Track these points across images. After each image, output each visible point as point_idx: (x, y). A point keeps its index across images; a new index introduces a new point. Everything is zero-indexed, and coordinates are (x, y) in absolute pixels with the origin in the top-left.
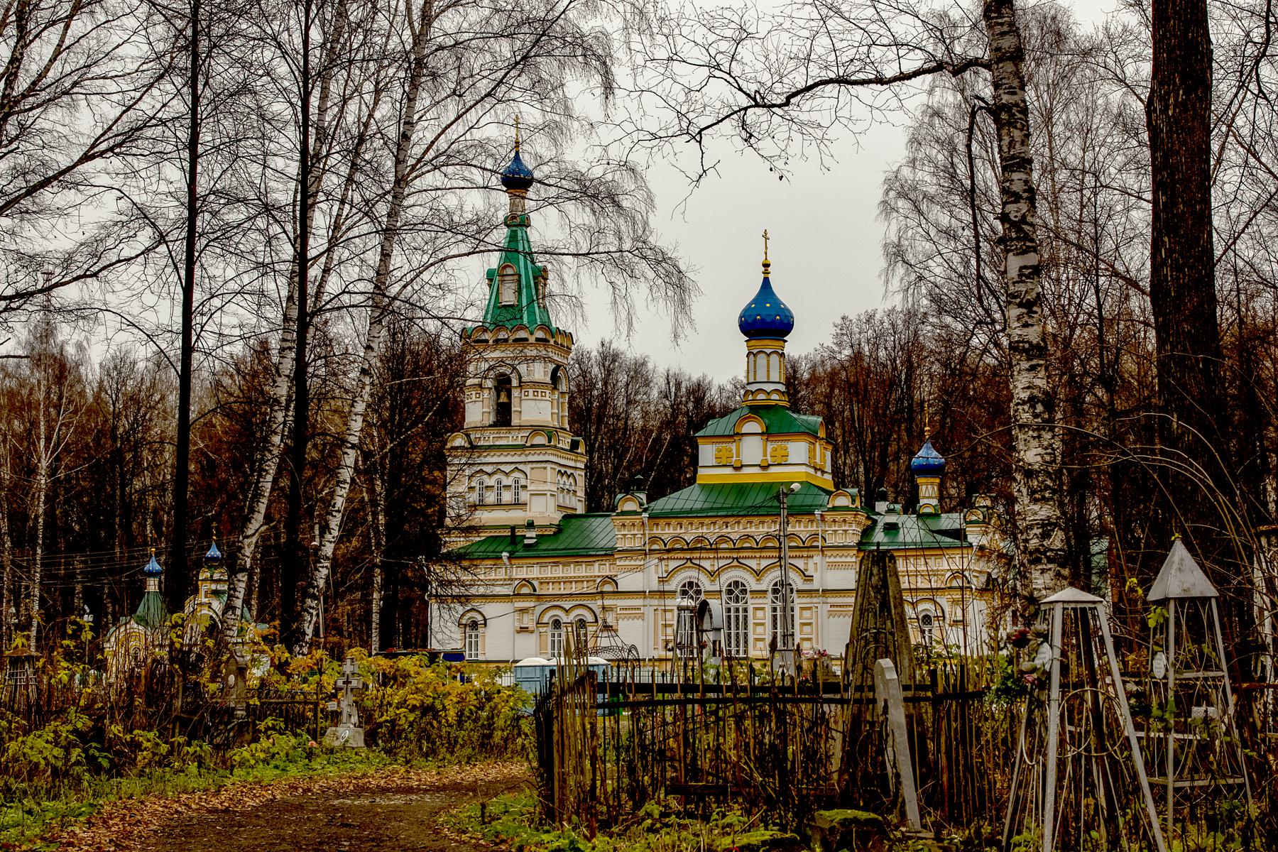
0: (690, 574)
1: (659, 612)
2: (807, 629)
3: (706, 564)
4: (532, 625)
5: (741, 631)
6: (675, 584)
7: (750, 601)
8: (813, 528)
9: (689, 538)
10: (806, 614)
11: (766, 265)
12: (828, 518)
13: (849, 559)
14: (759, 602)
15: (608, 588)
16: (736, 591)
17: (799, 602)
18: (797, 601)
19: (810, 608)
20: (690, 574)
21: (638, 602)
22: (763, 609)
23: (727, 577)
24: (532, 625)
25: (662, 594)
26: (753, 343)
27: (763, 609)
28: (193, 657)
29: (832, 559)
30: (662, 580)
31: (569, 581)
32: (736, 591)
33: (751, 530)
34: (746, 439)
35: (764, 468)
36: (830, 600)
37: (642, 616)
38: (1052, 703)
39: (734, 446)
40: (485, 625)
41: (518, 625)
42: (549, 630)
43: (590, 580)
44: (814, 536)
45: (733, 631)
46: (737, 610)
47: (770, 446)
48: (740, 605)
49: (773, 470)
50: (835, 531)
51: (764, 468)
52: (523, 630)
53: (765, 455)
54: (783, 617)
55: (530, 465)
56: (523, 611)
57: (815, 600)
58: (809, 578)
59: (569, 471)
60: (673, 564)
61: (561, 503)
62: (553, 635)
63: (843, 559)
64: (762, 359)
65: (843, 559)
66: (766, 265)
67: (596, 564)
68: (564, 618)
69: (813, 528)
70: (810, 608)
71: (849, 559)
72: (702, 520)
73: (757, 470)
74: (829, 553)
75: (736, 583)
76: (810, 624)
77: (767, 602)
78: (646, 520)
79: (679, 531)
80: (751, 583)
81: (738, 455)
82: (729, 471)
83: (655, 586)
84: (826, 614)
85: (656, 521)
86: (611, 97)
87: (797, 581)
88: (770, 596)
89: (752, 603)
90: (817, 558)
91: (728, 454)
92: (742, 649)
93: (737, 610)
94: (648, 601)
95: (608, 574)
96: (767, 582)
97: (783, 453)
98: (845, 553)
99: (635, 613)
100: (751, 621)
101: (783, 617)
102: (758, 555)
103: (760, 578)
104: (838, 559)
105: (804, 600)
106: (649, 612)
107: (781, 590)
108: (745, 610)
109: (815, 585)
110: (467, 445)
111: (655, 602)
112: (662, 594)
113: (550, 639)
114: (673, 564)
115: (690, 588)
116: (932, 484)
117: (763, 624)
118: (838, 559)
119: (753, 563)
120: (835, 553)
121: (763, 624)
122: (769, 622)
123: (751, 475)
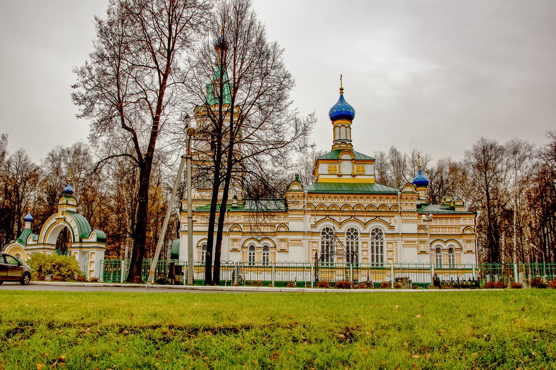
0: (328, 224)
1: (311, 243)
2: (390, 254)
3: (337, 219)
4: (239, 248)
5: (380, 254)
6: (319, 229)
7: (359, 239)
8: (395, 202)
11: (342, 89)
12: (404, 197)
13: (414, 218)
15: (282, 229)
16: (352, 233)
17: (385, 239)
18: (385, 239)
19: (391, 243)
20: (328, 224)
22: (366, 243)
24: (239, 248)
25: (313, 234)
26: (335, 123)
27: (366, 243)
29: (405, 218)
30: (312, 226)
32: (352, 233)
33: (361, 201)
34: (343, 162)
36: (404, 239)
37: (302, 245)
38: (154, 271)
41: (231, 248)
42: (247, 251)
44: (396, 206)
45: (375, 254)
46: (352, 243)
48: (379, 241)
49: (357, 177)
50: (406, 204)
51: (354, 176)
52: (235, 250)
54: (377, 250)
56: (235, 240)
57: (396, 239)
58: (392, 228)
60: (318, 218)
63: (411, 218)
64: (337, 129)
66: (342, 89)
68: (257, 244)
70: (391, 243)
71: (414, 218)
73: (350, 177)
74: (404, 215)
75: (352, 229)
76: (392, 251)
77: (369, 239)
78: (306, 194)
79: (322, 201)
80: (361, 229)
81: (340, 169)
82: (336, 177)
83: (309, 229)
84: (402, 246)
85: (311, 195)
87: (385, 229)
88: (346, 236)
89: (361, 239)
90: (397, 217)
91: (335, 169)
92: (380, 263)
93: (377, 243)
94: (306, 237)
96: (369, 229)
97: (363, 170)
98: (412, 215)
99: (299, 243)
100: (385, 250)
101: (377, 250)
102: (365, 215)
104: (408, 218)
105: (389, 239)
106: (305, 242)
107: (377, 233)
109: (396, 231)
110: (7, 257)
111: (309, 237)
112: (313, 234)
113: (248, 255)
114: (318, 218)
115: (327, 232)
117: (366, 251)
118: (408, 218)
119: (362, 219)
120: (407, 215)
121: (366, 251)
123: (347, 179)
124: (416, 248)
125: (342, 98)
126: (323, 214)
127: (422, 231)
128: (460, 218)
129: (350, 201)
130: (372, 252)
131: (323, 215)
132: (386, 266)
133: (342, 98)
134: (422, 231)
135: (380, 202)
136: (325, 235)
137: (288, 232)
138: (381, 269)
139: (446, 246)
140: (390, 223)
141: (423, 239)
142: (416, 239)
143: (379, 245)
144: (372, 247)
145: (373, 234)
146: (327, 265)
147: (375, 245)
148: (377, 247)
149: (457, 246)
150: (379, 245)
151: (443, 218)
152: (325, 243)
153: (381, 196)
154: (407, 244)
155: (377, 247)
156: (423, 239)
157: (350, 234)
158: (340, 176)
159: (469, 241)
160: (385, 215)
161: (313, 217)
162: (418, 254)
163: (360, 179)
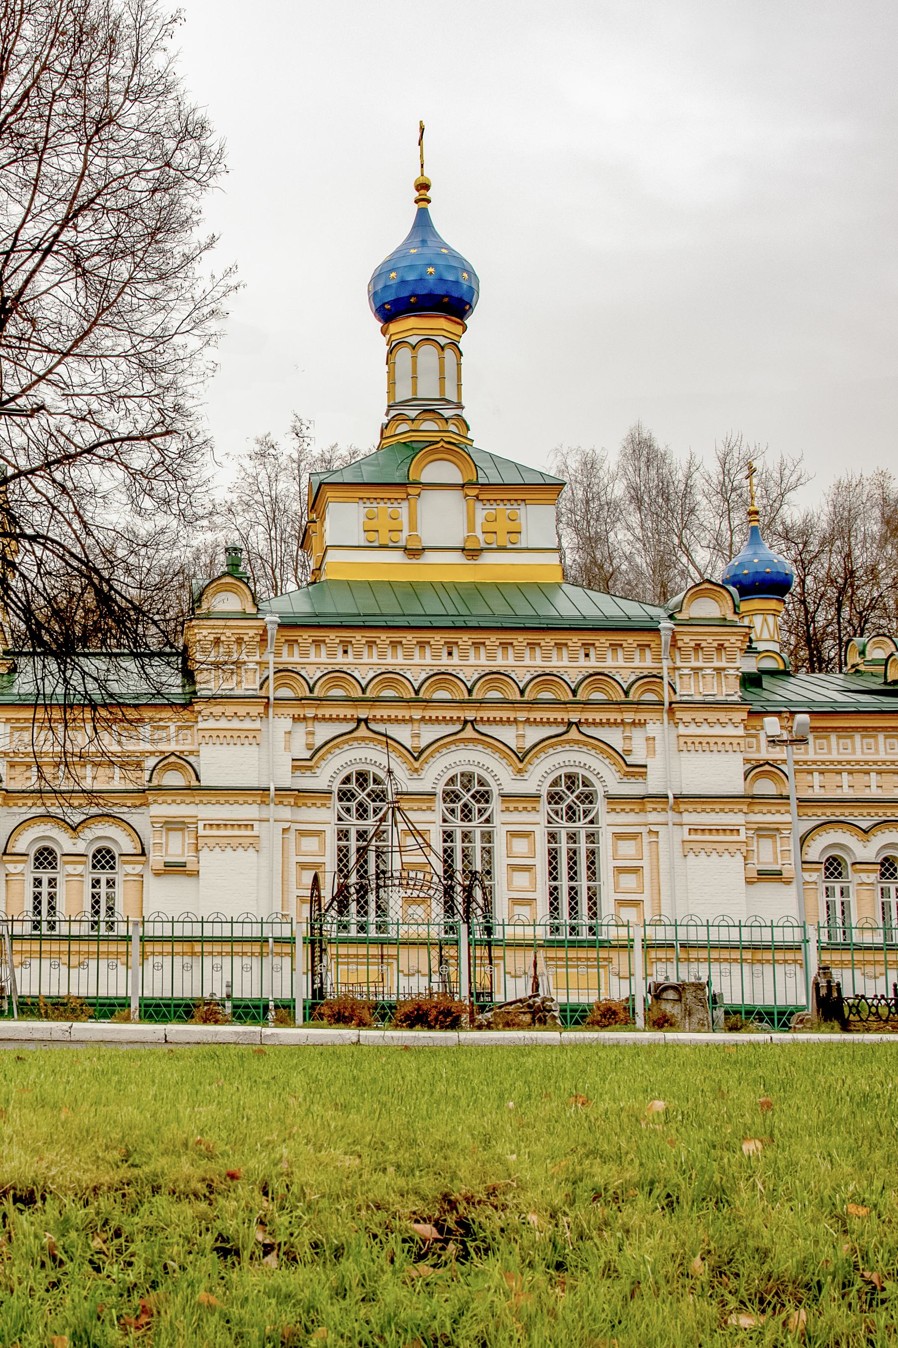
0: (367, 756)
1: (292, 835)
3: (402, 733)
5: (583, 883)
6: (328, 775)
7: (498, 819)
8: (646, 662)
9: (364, 675)
10: (627, 848)
11: (423, 186)
13: (730, 731)
14: (520, 819)
15: (173, 779)
16: (468, 797)
17: (608, 821)
19: (634, 836)
21: (248, 811)
26: (394, 327)
29: (693, 730)
31: (861, 769)
32: (468, 797)
36: (687, 818)
37: (254, 844)
39: (403, 510)
44: (652, 679)
45: (564, 884)
47: (481, 513)
49: (489, 558)
51: (472, 553)
53: (471, 526)
57: (653, 817)
58: (638, 771)
60: (324, 732)
62: (38, 882)
63: (718, 730)
64: (404, 354)
65: (718, 730)
66: (423, 186)
68: (64, 842)
69: (646, 662)
70: (634, 836)
71: (730, 731)
72: (396, 636)
73: (456, 558)
74: (687, 716)
76: (636, 870)
77: (537, 821)
78: (272, 630)
80: (502, 777)
81: (413, 526)
82: (397, 557)
85: (292, 634)
87: (608, 779)
89: (503, 820)
91: (394, 525)
93: (572, 837)
94: (274, 811)
95: (173, 747)
96: (538, 777)
97: (512, 527)
98: (723, 716)
99: (242, 837)
101: (572, 871)
102: (522, 716)
103: (516, 770)
104: (705, 730)
106: (269, 834)
107: (571, 797)
108: (488, 837)
109: (653, 785)
111: (286, 813)
113: (88, 890)
114: (324, 732)
115: (361, 792)
116: (775, 613)
117: (528, 868)
118: (705, 730)
119: (508, 735)
120: (700, 716)
121: (528, 868)
124: (739, 858)
125: (423, 221)
126: (342, 712)
127: (766, 787)
130: (553, 874)
131: (555, 722)
132: (609, 933)
133: (423, 221)
134: (766, 787)
136: (353, 805)
137: (196, 790)
138: (592, 945)
140: (629, 752)
141: (769, 818)
143: (583, 846)
144: (553, 855)
146: (362, 928)
147: (564, 846)
148: (573, 855)
150: (583, 846)
152: (353, 835)
154: (702, 841)
155: (573, 855)
156: (769, 818)
158: (414, 552)
161: (301, 728)
163: (498, 565)
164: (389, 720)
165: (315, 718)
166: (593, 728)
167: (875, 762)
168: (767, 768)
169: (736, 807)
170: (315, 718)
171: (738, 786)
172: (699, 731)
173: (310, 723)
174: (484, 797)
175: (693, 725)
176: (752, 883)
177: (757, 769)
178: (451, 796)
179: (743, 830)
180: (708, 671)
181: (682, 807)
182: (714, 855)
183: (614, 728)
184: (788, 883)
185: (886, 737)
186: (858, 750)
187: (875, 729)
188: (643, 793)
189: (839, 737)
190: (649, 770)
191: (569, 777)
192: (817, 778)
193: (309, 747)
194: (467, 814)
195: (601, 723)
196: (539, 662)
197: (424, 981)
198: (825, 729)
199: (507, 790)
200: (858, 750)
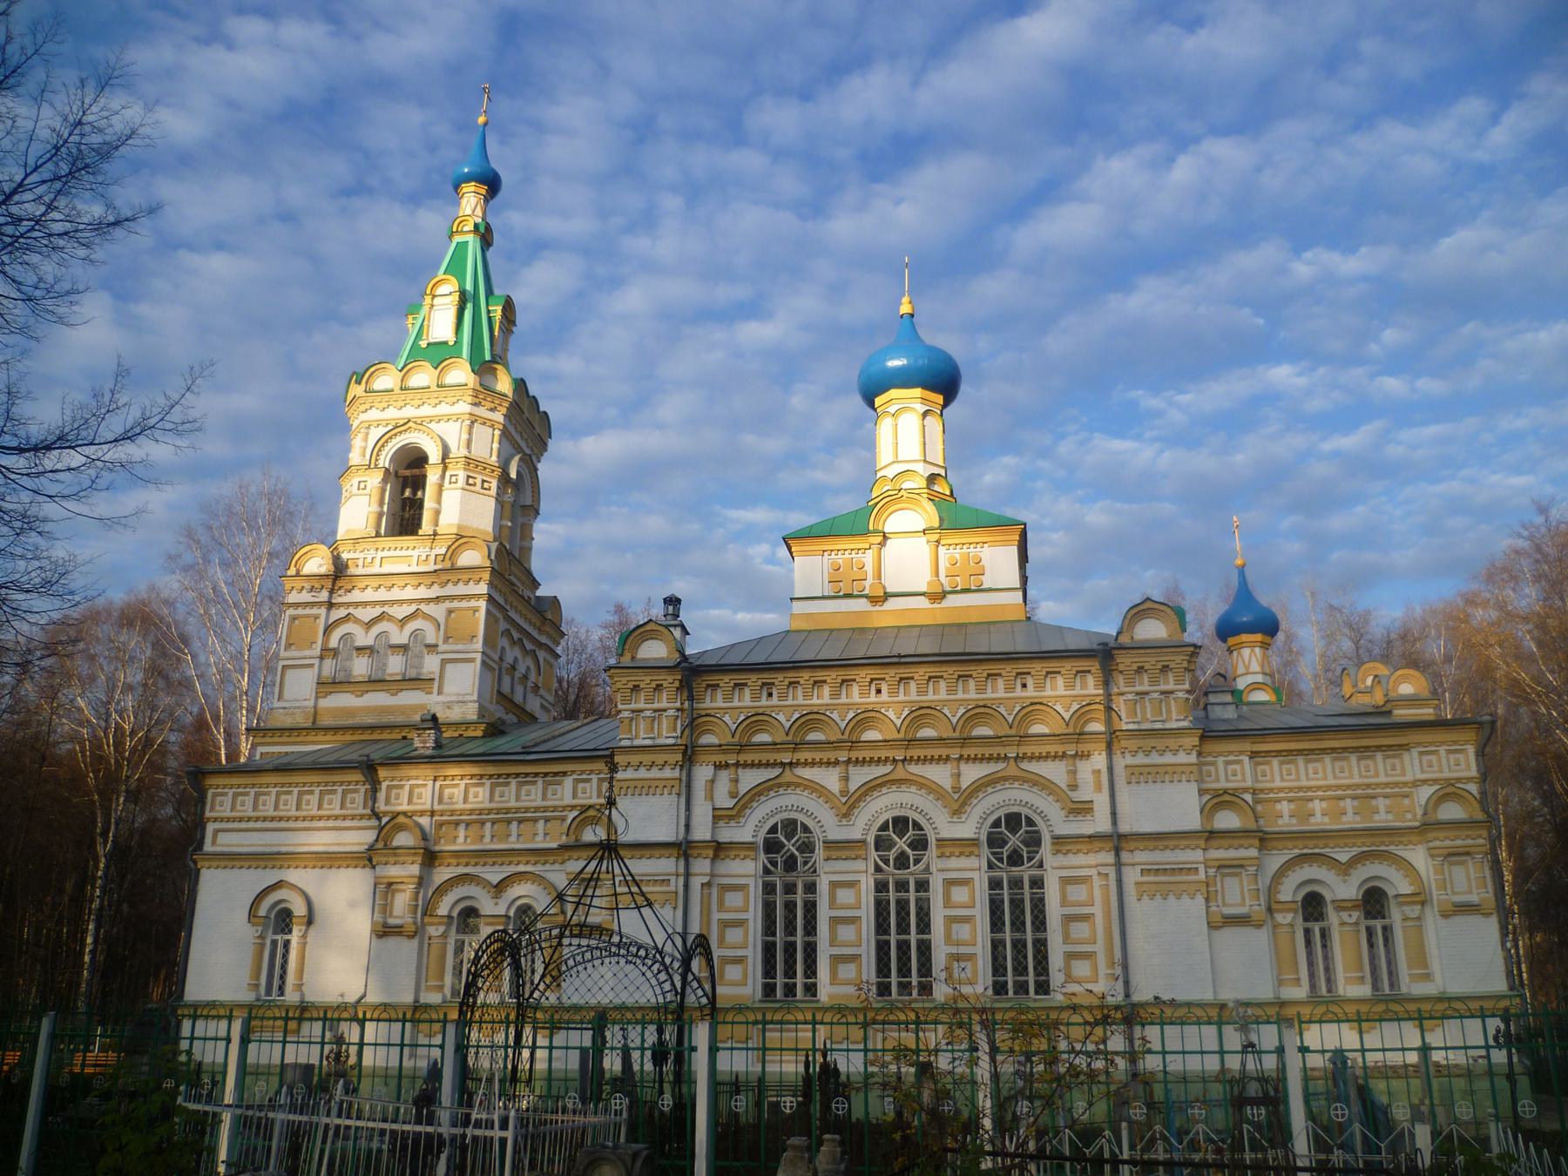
13: (1182, 758)
22: (852, 884)
23: (883, 806)
27: (852, 884)
28: (1272, 1093)
35: (943, 595)
36: (1215, 854)
40: (310, 921)
43: (549, 815)
48: (1026, 872)
49: (952, 601)
55: (448, 605)
59: (529, 646)
61: (506, 689)
67: (568, 782)
71: (1182, 758)
73: (923, 602)
77: (975, 869)
82: (861, 605)
86: (47, 527)
96: (864, 824)
100: (823, 913)
122: (981, 914)
124: (1200, 899)
127: (1227, 820)
128: (1405, 747)
129: (775, 701)
134: (1227, 820)
135: (1019, 692)
139: (1342, 888)
141: (1232, 853)
142: (1198, 855)
143: (799, 898)
145: (881, 844)
149: (1405, 887)
150: (799, 898)
151: (1300, 752)
153: (1023, 666)
156: (1232, 853)
157: (892, 844)
158: (875, 600)
159: (1453, 856)
160: (818, 756)
161: (724, 776)
162: (1212, 926)
164: (813, 764)
165: (737, 765)
166: (1034, 762)
167: (1349, 787)
168: (1226, 798)
169: (1194, 843)
170: (737, 765)
171: (1194, 822)
172: (1147, 761)
173: (733, 769)
174: (920, 844)
175: (1141, 755)
176: (1217, 928)
177: (1220, 800)
178: (771, 846)
179: (1202, 868)
180: (1155, 695)
181: (947, 851)
182: (1172, 898)
183: (1057, 762)
184: (1259, 926)
185: (1360, 759)
186: (1303, 777)
187: (1345, 749)
188: (1090, 831)
189: (1386, 757)
190: (1096, 806)
191: (896, 820)
192: (1381, 803)
193: (733, 795)
194: (902, 862)
195: (1040, 758)
196: (973, 695)
197: (199, 1033)
198: (1367, 748)
199: (831, 837)
200: (1330, 775)
